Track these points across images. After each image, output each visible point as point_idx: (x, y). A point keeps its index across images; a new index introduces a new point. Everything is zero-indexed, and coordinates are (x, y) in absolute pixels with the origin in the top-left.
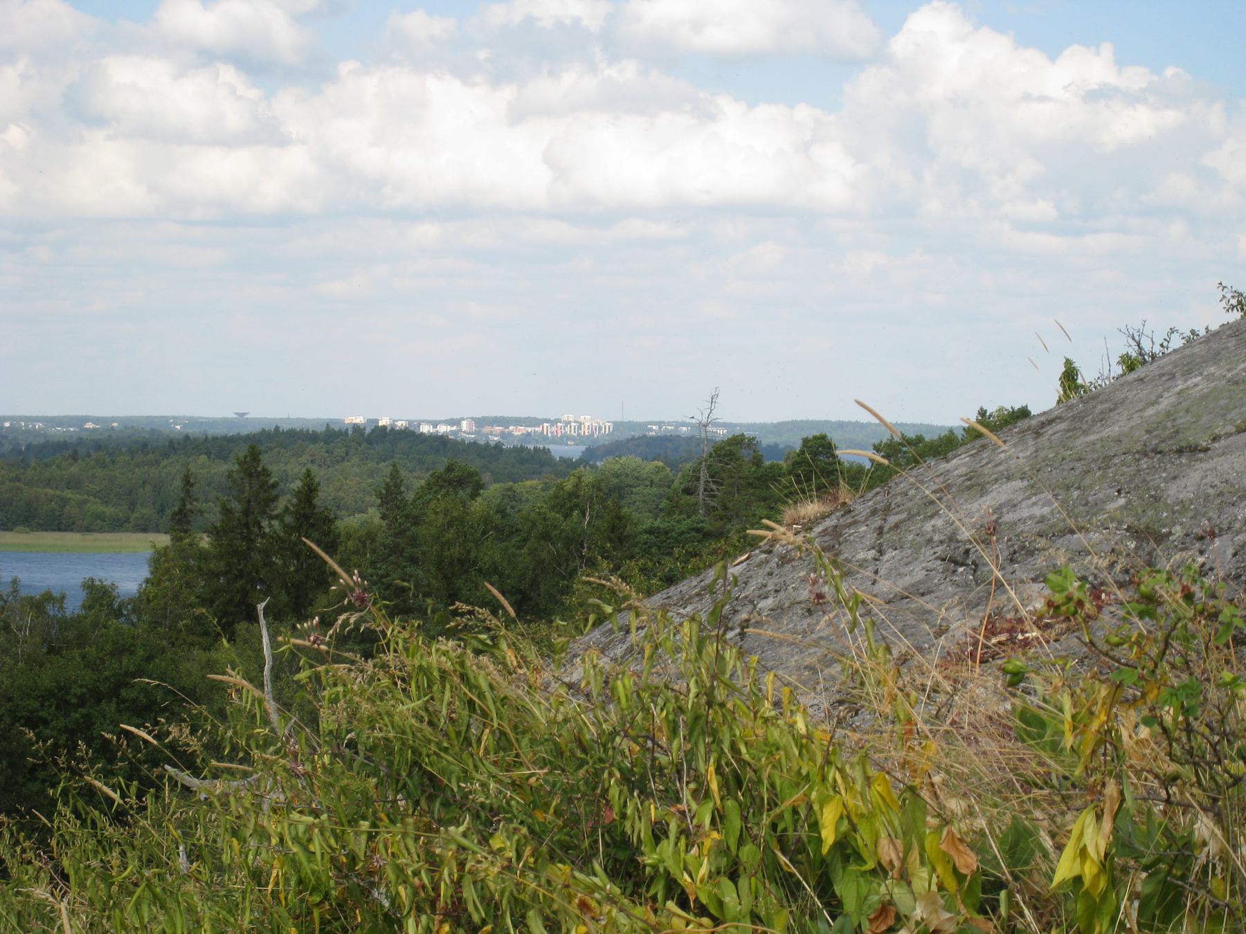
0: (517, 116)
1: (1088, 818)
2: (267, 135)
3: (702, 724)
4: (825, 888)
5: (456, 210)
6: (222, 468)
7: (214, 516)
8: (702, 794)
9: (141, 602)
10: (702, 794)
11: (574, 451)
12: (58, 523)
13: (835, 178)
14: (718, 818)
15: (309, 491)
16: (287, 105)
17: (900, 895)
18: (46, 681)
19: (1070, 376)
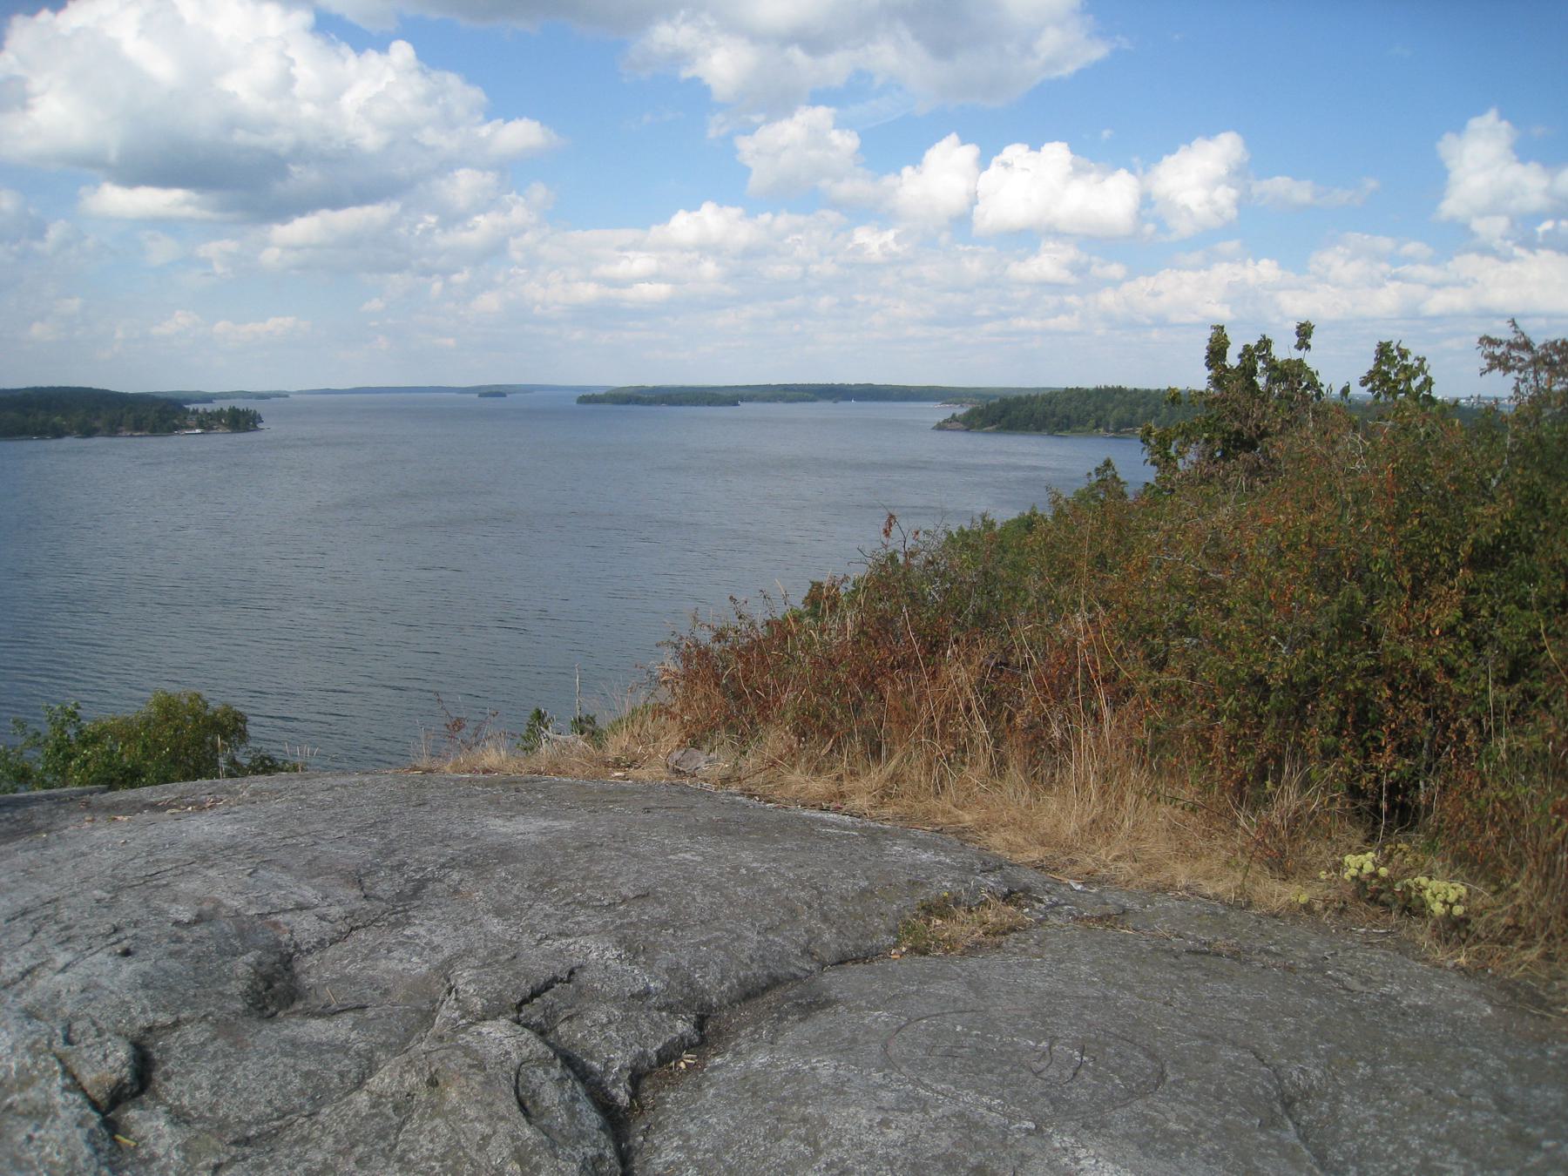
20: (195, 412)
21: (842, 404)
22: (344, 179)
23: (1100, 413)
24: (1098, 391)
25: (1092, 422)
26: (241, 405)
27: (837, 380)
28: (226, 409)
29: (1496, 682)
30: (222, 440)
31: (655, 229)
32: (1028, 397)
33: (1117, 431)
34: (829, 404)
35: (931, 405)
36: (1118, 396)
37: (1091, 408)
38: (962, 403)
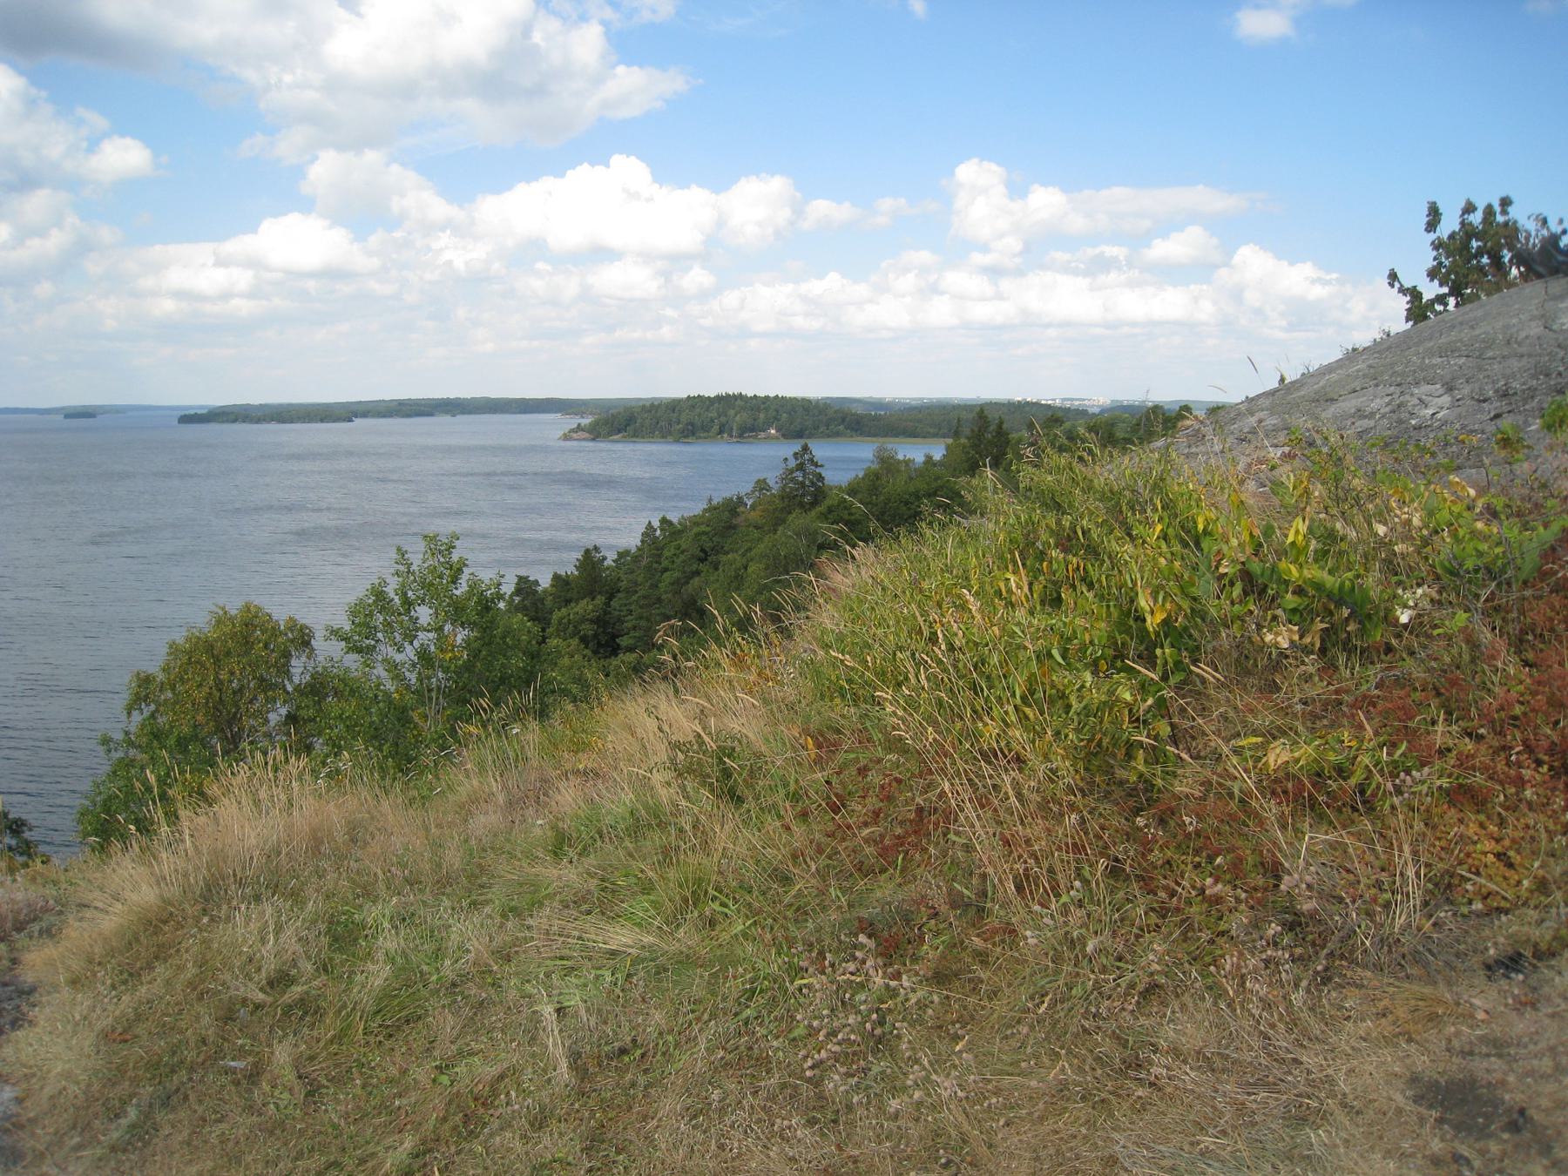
1: (1300, 519)
2: (999, 297)
3: (1158, 486)
4: (1197, 544)
5: (1066, 324)
6: (971, 416)
7: (967, 431)
8: (1155, 510)
9: (941, 463)
10: (1155, 510)
11: (1097, 410)
13: (1206, 311)
14: (1161, 519)
16: (1006, 285)
17: (1225, 548)
18: (912, 489)
19: (1282, 380)
21: (460, 418)
23: (723, 419)
24: (719, 399)
26: (1060, 414)
27: (452, 394)
29: (1043, 603)
31: (158, 248)
32: (652, 405)
33: (741, 436)
34: (448, 418)
36: (739, 402)
38: (582, 414)
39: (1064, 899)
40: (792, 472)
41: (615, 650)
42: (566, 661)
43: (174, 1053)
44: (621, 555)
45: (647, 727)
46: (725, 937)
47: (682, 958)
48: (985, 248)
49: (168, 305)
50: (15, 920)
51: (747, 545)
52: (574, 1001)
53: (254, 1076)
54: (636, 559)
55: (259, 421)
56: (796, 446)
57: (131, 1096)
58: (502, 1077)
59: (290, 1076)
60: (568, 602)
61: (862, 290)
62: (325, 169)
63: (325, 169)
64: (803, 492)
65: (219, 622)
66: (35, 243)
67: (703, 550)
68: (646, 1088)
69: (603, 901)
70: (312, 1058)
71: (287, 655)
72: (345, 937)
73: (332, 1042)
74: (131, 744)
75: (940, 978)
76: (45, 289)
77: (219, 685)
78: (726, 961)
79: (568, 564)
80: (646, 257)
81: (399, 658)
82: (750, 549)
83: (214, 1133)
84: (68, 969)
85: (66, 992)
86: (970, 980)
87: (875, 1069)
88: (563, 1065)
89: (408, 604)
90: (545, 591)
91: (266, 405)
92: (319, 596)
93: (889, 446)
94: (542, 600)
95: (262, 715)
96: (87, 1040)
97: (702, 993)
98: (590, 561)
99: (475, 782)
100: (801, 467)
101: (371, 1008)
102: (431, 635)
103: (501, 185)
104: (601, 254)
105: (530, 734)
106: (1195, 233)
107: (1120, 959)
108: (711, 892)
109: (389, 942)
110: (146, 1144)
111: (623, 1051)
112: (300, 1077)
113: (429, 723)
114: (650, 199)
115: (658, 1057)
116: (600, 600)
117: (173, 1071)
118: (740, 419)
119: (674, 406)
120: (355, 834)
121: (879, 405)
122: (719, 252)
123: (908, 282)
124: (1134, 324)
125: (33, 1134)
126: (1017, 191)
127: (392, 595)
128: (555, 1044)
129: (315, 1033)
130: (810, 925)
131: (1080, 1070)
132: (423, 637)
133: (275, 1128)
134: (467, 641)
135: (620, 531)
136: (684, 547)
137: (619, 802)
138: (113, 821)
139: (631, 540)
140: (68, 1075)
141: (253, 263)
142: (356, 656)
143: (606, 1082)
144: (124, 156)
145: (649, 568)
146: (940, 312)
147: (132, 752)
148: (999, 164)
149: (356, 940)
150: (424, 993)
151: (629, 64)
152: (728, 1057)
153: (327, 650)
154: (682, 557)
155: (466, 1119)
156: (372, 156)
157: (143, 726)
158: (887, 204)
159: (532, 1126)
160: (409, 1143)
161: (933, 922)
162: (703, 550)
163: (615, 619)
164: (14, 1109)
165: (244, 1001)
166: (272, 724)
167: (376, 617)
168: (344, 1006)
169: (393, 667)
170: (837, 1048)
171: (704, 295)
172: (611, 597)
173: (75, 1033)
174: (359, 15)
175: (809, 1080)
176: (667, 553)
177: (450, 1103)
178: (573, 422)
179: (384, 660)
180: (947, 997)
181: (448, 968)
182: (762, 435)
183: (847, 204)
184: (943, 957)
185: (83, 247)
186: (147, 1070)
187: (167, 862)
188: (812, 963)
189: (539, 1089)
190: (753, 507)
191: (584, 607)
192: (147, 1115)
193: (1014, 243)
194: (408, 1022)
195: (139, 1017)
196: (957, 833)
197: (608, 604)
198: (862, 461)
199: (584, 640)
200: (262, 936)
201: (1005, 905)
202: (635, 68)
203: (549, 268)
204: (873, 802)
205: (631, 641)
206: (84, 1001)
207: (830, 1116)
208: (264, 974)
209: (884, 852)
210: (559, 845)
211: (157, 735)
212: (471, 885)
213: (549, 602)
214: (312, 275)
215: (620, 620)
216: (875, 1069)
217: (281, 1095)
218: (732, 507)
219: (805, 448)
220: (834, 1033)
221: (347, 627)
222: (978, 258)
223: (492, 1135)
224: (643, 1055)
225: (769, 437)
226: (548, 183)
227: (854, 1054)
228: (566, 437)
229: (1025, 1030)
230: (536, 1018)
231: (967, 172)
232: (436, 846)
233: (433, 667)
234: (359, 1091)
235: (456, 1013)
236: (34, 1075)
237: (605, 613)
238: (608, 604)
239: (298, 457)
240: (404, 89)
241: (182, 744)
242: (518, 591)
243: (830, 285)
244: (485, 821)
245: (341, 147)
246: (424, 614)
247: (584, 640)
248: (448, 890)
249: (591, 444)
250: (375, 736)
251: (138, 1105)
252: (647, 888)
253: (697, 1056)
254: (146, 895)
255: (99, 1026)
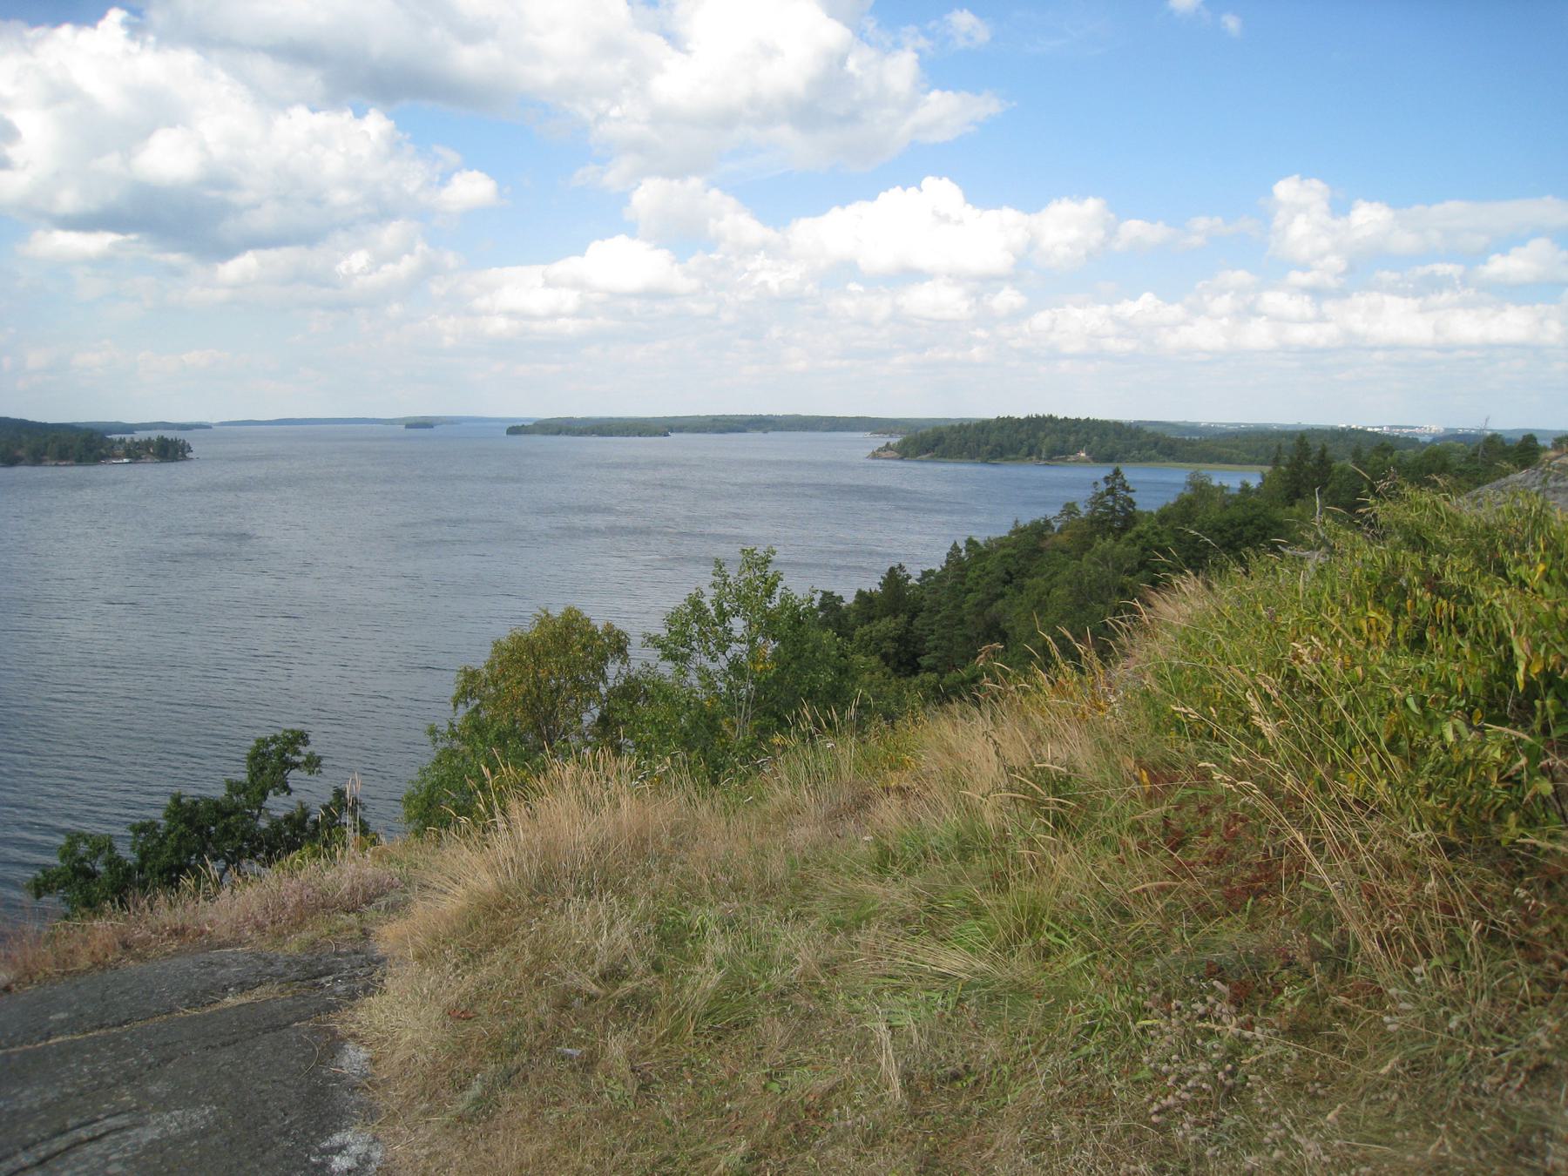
0: (1423, 310)
2: (1321, 319)
5: (1393, 347)
6: (1291, 443)
7: (1286, 458)
8: (1536, 549)
9: (1257, 492)
10: (1536, 549)
11: (1428, 439)
12: (1229, 461)
14: (1543, 558)
15: (1324, 450)
16: (1329, 307)
18: (1226, 516)
20: (122, 441)
21: (771, 434)
22: (307, 226)
23: (1032, 441)
24: (1029, 420)
25: (1025, 449)
26: (169, 435)
28: (154, 438)
30: (153, 473)
31: (494, 270)
32: (961, 426)
34: (759, 435)
35: (860, 435)
37: (1024, 436)
38: (891, 433)
39: (1436, 961)
40: (1102, 496)
41: (915, 669)
42: (866, 677)
43: (514, 1034)
44: (925, 574)
45: (973, 754)
46: (1059, 969)
47: (1015, 986)
48: (1305, 268)
49: (500, 324)
50: (365, 893)
51: (1052, 569)
52: (907, 1020)
53: (589, 1064)
54: (940, 578)
55: (581, 433)
56: (1105, 470)
57: (475, 1071)
58: (833, 1091)
59: (624, 1068)
60: (870, 619)
61: (1176, 311)
62: (648, 195)
63: (648, 195)
64: (1114, 516)
65: (542, 623)
66: (388, 269)
67: (1008, 573)
68: (981, 1116)
69: (931, 921)
70: (645, 1053)
71: (604, 659)
72: (674, 939)
73: (663, 1038)
74: (455, 735)
75: (1297, 1032)
76: (395, 309)
77: (538, 683)
78: (1062, 997)
79: (872, 584)
80: (957, 278)
81: (712, 667)
82: (1055, 574)
83: (553, 1114)
84: (415, 945)
85: (415, 966)
86: (1329, 1038)
87: (1228, 1122)
88: (897, 1084)
89: (723, 615)
90: (849, 607)
91: (587, 419)
92: (634, 600)
93: (1204, 473)
94: (845, 616)
95: (576, 714)
96: (436, 1013)
97: (1037, 1025)
98: (894, 579)
99: (788, 793)
100: (1111, 492)
101: (702, 1010)
102: (744, 646)
103: (819, 209)
104: (910, 276)
105: (843, 751)
106: (1540, 246)
107: (1500, 1031)
108: (1047, 921)
109: (717, 947)
110: (490, 1118)
111: (956, 1077)
112: (633, 1070)
113: (739, 732)
114: (959, 222)
115: (993, 1085)
116: (903, 618)
117: (514, 1052)
118: (1047, 443)
119: (984, 426)
120: (682, 836)
121: (1193, 429)
122: (1031, 273)
123: (1223, 304)
124: (1469, 347)
125: (387, 1096)
126: (1340, 208)
127: (708, 605)
128: (889, 1066)
129: (647, 1029)
130: (1157, 964)
131: (1460, 1149)
132: (735, 648)
133: (612, 1116)
134: (776, 652)
135: (923, 549)
136: (989, 568)
137: (943, 824)
138: (442, 806)
139: (936, 561)
140: (415, 1044)
141: (578, 284)
142: (670, 664)
143: (939, 1106)
144: (472, 188)
145: (952, 588)
146: (1258, 334)
147: (456, 743)
148: (1306, 175)
149: (682, 941)
150: (752, 999)
151: (943, 89)
152: (1066, 1093)
153: (642, 657)
154: (987, 579)
155: (798, 1129)
156: (695, 182)
157: (467, 719)
158: (1201, 223)
159: (865, 1142)
160: (743, 1146)
161: (1286, 972)
162: (1008, 573)
163: (921, 643)
164: (370, 1070)
165: (579, 993)
166: (585, 724)
167: (691, 628)
168: (676, 1006)
169: (705, 674)
170: (1185, 1096)
171: (1016, 316)
172: (913, 616)
173: (423, 1005)
174: (688, 52)
175: (1155, 1126)
176: (971, 574)
177: (781, 1111)
178: (881, 441)
179: (699, 669)
180: (1307, 1053)
181: (776, 977)
182: (1072, 458)
183: (1161, 224)
184: (1301, 1009)
185: (430, 270)
186: (489, 1048)
187: (502, 845)
188: (1157, 1005)
189: (870, 1106)
190: (1061, 531)
191: (887, 625)
192: (490, 1090)
193: (1335, 262)
194: (737, 1026)
195: (480, 997)
196: (1310, 880)
197: (910, 623)
198: (1175, 485)
199: (885, 657)
200: (601, 930)
201: (1368, 960)
202: (950, 93)
203: (861, 289)
204: (1214, 842)
205: (932, 661)
206: (431, 978)
207: (1179, 1166)
208: (597, 967)
209: (1230, 897)
210: (884, 861)
211: (479, 728)
212: (793, 894)
213: (852, 618)
214: (637, 295)
215: (922, 640)
216: (1228, 1122)
217: (618, 1089)
218: (1040, 530)
219: (1117, 473)
220: (1181, 1079)
221: (664, 633)
222: (1297, 278)
223: (823, 1148)
224: (977, 1082)
225: (1078, 461)
226: (859, 208)
227: (1204, 1103)
228: (874, 456)
229: (1395, 1097)
230: (866, 1038)
231: (1285, 189)
232: (761, 853)
233: (744, 677)
234: (689, 1089)
235: (785, 1022)
236: (385, 1040)
237: (907, 631)
238: (910, 623)
239: (618, 466)
240: (725, 119)
241: (501, 738)
242: (823, 606)
243: (1142, 306)
244: (802, 834)
245: (669, 175)
246: (738, 625)
247: (885, 657)
248: (772, 899)
249: (899, 463)
250: (687, 743)
251: (483, 1080)
252: (978, 912)
253: (1035, 1089)
254: (486, 882)
255: (445, 1001)
